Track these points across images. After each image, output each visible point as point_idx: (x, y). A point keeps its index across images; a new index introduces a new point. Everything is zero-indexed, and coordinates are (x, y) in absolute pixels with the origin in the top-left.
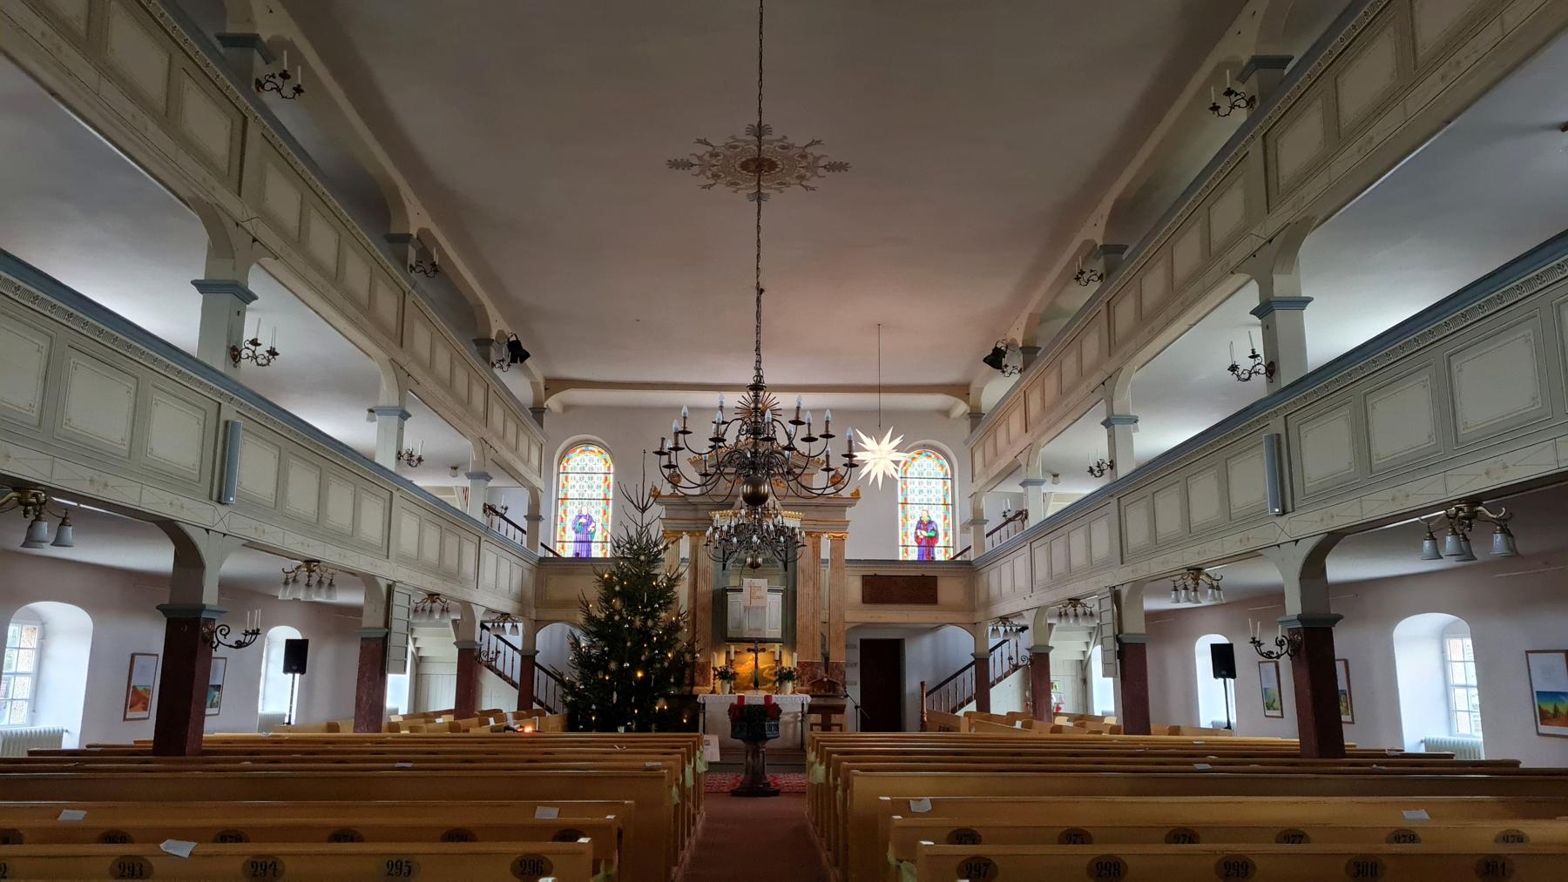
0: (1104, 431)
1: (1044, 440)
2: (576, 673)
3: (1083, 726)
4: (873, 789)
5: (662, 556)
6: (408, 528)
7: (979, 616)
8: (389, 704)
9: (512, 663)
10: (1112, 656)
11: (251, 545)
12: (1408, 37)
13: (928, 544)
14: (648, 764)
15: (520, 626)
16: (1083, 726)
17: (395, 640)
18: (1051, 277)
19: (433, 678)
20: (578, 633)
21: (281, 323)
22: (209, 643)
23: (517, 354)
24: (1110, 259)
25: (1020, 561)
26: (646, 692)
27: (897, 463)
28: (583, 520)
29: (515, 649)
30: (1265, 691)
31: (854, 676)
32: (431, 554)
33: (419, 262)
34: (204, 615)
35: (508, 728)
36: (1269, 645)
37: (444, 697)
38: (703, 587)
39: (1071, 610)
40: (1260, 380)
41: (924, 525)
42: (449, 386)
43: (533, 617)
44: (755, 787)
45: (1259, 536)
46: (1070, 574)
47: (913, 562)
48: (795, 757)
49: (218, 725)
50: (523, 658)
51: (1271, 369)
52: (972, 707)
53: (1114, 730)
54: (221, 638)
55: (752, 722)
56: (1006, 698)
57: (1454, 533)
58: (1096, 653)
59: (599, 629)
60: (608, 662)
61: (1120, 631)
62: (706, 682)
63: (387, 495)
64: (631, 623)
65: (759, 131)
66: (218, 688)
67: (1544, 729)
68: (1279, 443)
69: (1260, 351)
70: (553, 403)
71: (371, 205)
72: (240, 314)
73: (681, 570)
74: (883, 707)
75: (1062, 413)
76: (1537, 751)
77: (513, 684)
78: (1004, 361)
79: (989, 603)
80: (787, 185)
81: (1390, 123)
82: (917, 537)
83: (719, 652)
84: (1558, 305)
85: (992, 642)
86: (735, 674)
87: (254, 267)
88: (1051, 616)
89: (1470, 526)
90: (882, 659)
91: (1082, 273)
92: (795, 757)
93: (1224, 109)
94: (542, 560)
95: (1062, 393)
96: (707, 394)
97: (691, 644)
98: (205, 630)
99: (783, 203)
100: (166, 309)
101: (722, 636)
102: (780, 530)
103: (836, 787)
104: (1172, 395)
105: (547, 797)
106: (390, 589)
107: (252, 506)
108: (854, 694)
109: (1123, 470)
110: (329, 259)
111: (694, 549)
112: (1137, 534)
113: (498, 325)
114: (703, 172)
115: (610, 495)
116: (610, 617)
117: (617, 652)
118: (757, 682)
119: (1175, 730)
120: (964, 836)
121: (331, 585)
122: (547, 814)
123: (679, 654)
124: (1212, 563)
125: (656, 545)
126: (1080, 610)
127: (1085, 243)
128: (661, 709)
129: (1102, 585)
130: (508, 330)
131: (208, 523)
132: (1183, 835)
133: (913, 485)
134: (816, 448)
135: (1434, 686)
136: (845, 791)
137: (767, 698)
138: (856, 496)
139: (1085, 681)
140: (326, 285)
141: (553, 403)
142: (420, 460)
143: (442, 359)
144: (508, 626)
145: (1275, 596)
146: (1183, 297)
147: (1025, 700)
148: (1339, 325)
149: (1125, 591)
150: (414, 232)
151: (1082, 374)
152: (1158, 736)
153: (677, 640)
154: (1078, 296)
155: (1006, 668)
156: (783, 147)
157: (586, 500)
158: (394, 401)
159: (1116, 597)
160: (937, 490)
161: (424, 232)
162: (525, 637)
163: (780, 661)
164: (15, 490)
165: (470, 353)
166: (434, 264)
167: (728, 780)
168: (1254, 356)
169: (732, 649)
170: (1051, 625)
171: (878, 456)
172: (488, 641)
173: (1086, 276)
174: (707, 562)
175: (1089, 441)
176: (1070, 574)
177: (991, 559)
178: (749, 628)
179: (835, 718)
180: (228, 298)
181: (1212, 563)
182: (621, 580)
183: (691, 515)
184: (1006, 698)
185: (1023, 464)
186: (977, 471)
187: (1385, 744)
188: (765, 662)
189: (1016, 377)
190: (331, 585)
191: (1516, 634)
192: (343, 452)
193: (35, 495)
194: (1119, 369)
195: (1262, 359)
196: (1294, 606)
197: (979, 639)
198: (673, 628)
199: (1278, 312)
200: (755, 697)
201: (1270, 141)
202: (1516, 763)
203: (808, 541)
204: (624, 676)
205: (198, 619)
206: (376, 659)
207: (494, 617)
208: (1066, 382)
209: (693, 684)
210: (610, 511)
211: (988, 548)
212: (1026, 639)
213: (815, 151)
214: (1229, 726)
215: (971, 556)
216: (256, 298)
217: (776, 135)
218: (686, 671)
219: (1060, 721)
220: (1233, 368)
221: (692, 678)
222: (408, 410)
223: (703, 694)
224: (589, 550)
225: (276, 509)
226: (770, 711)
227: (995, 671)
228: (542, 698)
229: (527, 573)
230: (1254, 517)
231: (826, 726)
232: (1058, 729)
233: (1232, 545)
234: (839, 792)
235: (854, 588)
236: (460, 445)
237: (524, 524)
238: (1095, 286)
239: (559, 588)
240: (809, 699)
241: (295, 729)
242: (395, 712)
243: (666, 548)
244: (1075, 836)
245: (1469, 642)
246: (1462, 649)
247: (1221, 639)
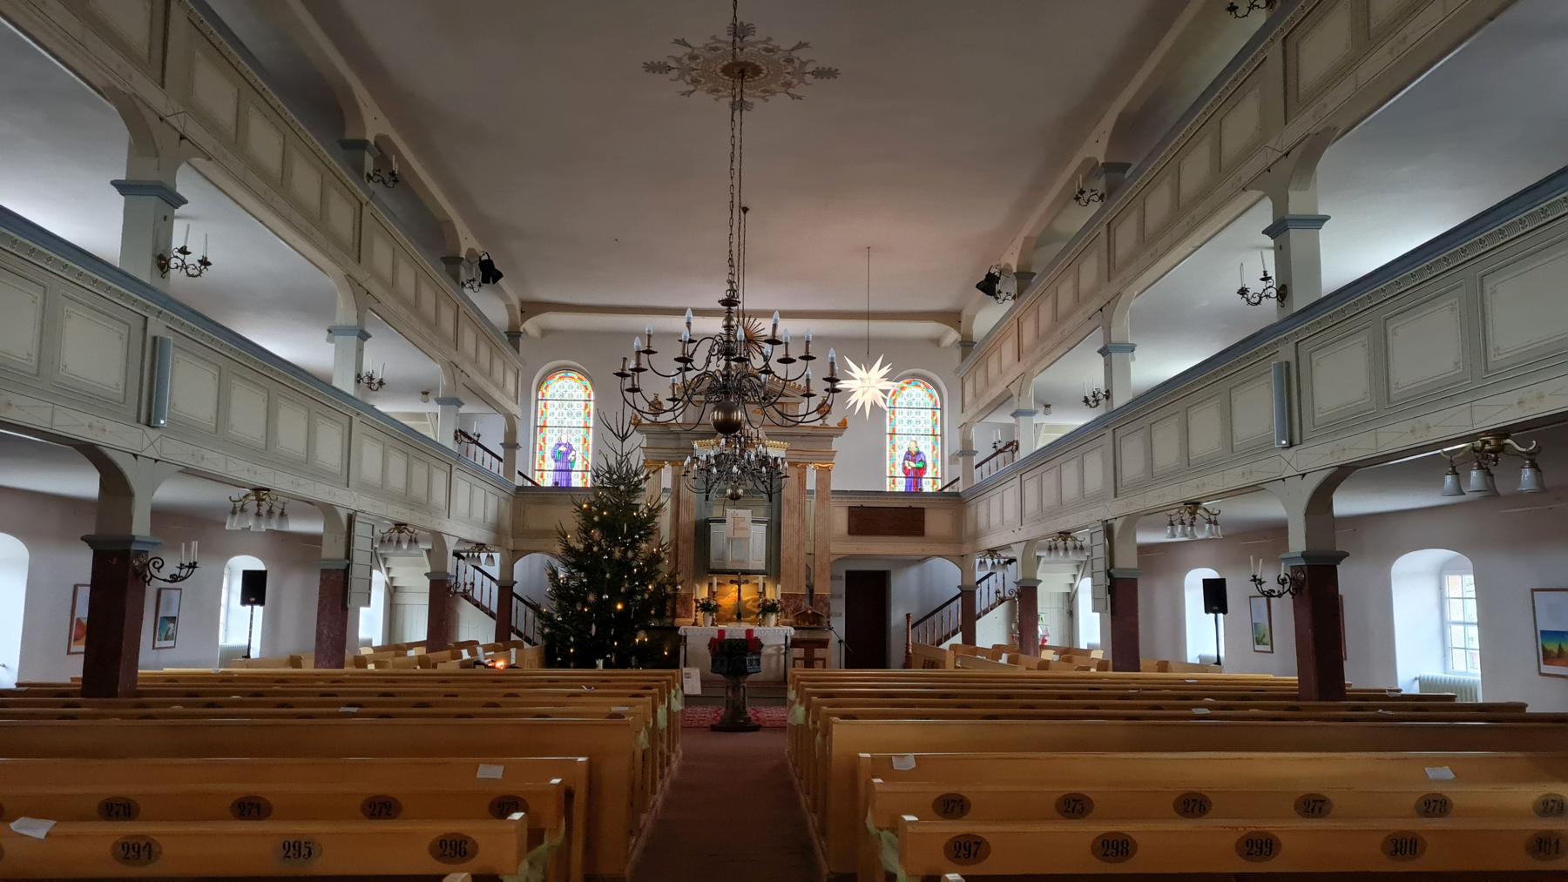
0: (1101, 360)
1: (1037, 369)
2: (555, 605)
3: (1069, 660)
4: (853, 738)
5: (643, 486)
6: (370, 458)
7: (966, 549)
8: (363, 634)
9: (488, 593)
10: (1103, 591)
11: (189, 472)
12: (1177, 188)
13: (915, 475)
14: (615, 709)
15: (497, 556)
16: (1069, 660)
17: (357, 572)
18: (1042, 208)
20: (556, 563)
21: (219, 237)
22: (142, 578)
23: (490, 274)
24: (1112, 176)
25: (1010, 494)
26: (626, 624)
27: (885, 392)
28: (563, 449)
29: (492, 579)
30: (1255, 626)
32: (397, 481)
34: (134, 547)
35: (478, 663)
36: (1271, 583)
37: (417, 628)
38: (687, 518)
39: (1061, 543)
40: (1271, 304)
41: (912, 455)
42: (415, 306)
43: (511, 546)
44: (736, 722)
45: (1263, 470)
46: (1061, 507)
47: (900, 493)
48: (776, 690)
49: (156, 660)
50: (501, 589)
51: (1283, 293)
52: (957, 639)
53: (1102, 666)
55: (733, 657)
56: (992, 630)
57: (1480, 467)
58: (1085, 587)
59: (576, 560)
60: (586, 594)
61: (1112, 566)
62: (688, 613)
63: (345, 420)
64: (610, 554)
65: (739, 31)
66: (173, 619)
67: (1546, 669)
68: (1288, 369)
69: (1272, 273)
70: (530, 326)
71: (320, 107)
72: (167, 220)
73: (663, 500)
74: (869, 644)
75: (1056, 341)
76: (1544, 695)
77: (491, 615)
78: (998, 287)
79: (976, 536)
80: (772, 93)
81: (1344, 90)
82: (905, 468)
83: (701, 583)
85: (979, 575)
86: (717, 607)
87: (184, 168)
88: (1040, 549)
89: (1496, 460)
90: (868, 590)
91: (1082, 192)
92: (776, 690)
93: (1242, 11)
94: (518, 488)
95: (1057, 320)
96: (685, 312)
97: (672, 576)
98: (136, 563)
99: (770, 113)
100: (87, 218)
101: (705, 567)
102: (764, 460)
103: (816, 731)
104: (1170, 324)
105: (492, 751)
106: (351, 519)
107: (186, 430)
108: (838, 626)
109: (1119, 400)
110: (272, 161)
111: (676, 480)
112: (1132, 466)
113: (468, 242)
114: (681, 76)
115: (591, 424)
116: (589, 547)
117: (595, 584)
118: (739, 614)
119: (1163, 666)
120: (952, 806)
121: (282, 514)
122: (490, 771)
123: (660, 586)
124: (1208, 498)
125: (636, 475)
126: (1070, 543)
127: (1086, 161)
128: (642, 642)
129: (1093, 519)
130: (479, 249)
131: (137, 449)
132: (1193, 804)
133: (901, 415)
134: (793, 371)
135: (1432, 625)
136: (824, 736)
137: (749, 632)
138: (843, 425)
139: (1071, 614)
140: (270, 193)
141: (530, 326)
142: (381, 383)
143: (406, 279)
144: (483, 556)
145: (1278, 531)
146: (1190, 217)
147: (1011, 633)
148: (1354, 249)
149: (1117, 525)
151: (1078, 300)
152: (1147, 673)
153: (659, 572)
154: (1077, 218)
155: (993, 600)
156: (767, 50)
157: (566, 425)
158: (353, 321)
159: (1109, 531)
160: (926, 420)
161: (382, 141)
162: (502, 567)
163: (764, 592)
166: (393, 174)
167: (710, 713)
168: (1266, 278)
169: (715, 581)
170: (1039, 558)
171: (865, 385)
172: (467, 574)
173: (1086, 196)
174: (691, 496)
175: (1085, 371)
176: (1061, 507)
177: (979, 491)
178: (732, 560)
179: (819, 653)
180: (151, 203)
181: (1208, 498)
182: (600, 510)
183: (672, 444)
184: (992, 630)
185: (1015, 394)
186: (967, 400)
187: (1378, 683)
188: (748, 594)
189: (1010, 303)
190: (282, 514)
191: (1521, 573)
192: (293, 373)
194: (1119, 294)
195: (1273, 282)
196: (1297, 543)
197: (967, 571)
198: (654, 559)
199: (1293, 232)
200: (736, 630)
202: (1522, 707)
203: (793, 473)
204: (603, 608)
206: (338, 596)
207: (468, 547)
208: (1151, 224)
209: (674, 616)
210: (590, 439)
211: (977, 480)
212: (1013, 574)
213: (802, 55)
214: (1218, 662)
215: (959, 487)
216: (185, 202)
217: (760, 35)
218: (667, 604)
219: (1047, 655)
220: (1243, 291)
221: (674, 610)
222: (367, 330)
223: (685, 626)
224: (569, 480)
225: (219, 432)
226: (752, 645)
227: (981, 603)
228: (521, 628)
230: (1259, 450)
231: (809, 662)
232: (1045, 665)
233: (1234, 479)
234: (819, 738)
235: (840, 520)
236: (426, 368)
237: (500, 452)
238: (1095, 207)
239: (538, 518)
240: (791, 631)
241: (257, 663)
242: (368, 643)
243: (647, 478)
244: (1074, 806)
245: (1470, 578)
246: (1462, 586)
247: (1212, 574)
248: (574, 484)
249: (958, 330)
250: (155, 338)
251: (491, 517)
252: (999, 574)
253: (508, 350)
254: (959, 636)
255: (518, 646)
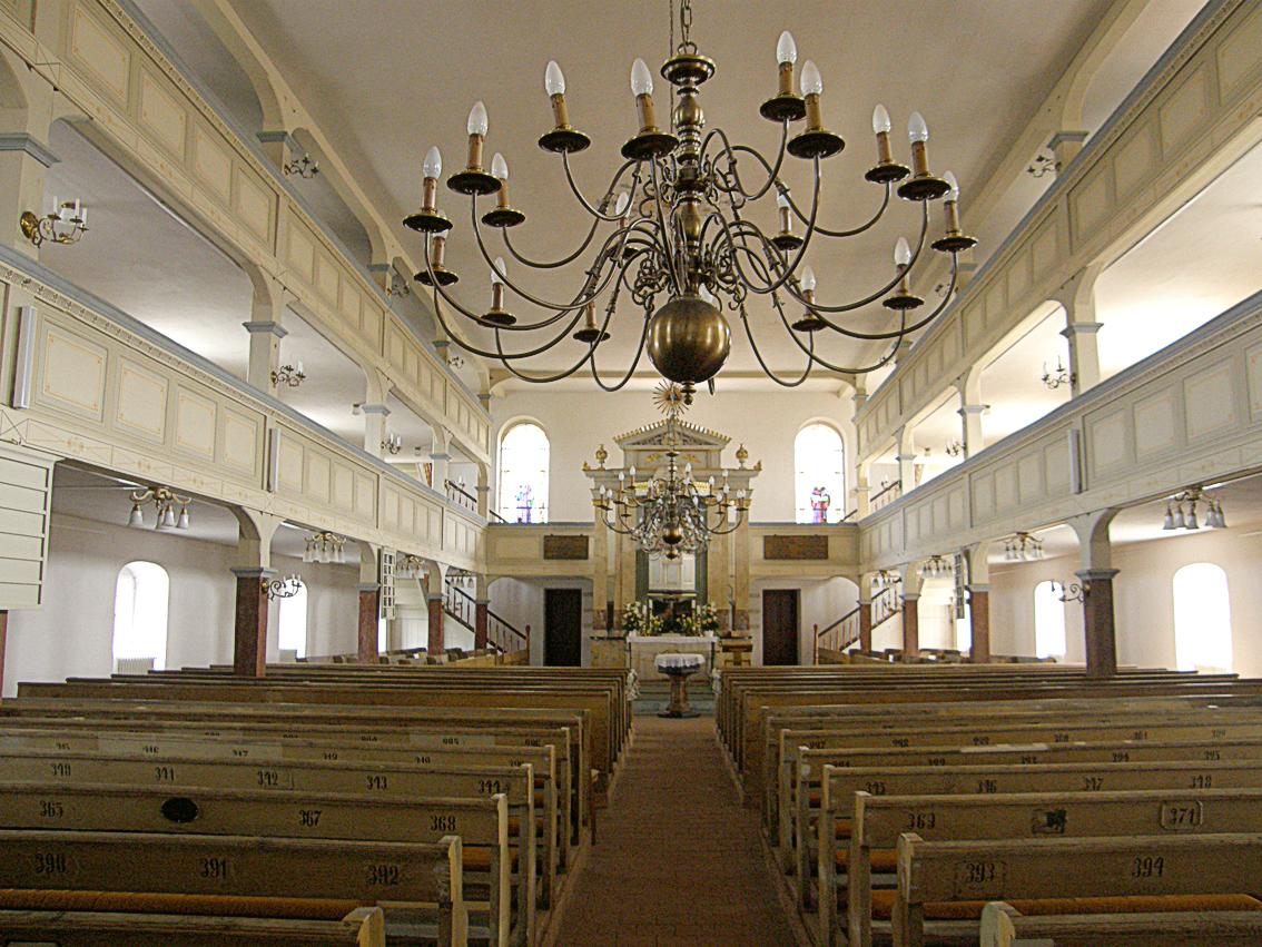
12: (1158, 137)
19: (404, 623)
29: (470, 599)
31: (757, 619)
32: (407, 523)
33: (394, 287)
34: (263, 575)
39: (933, 564)
41: (818, 491)
51: (1074, 380)
54: (275, 591)
56: (886, 637)
63: (375, 477)
68: (1078, 436)
77: (470, 628)
79: (872, 558)
84: (1246, 349)
85: (875, 592)
90: (783, 607)
126: (941, 564)
138: (758, 468)
141: (497, 389)
144: (466, 579)
150: (390, 263)
164: (150, 489)
165: (431, 353)
166: (406, 288)
179: (744, 656)
186: (862, 445)
193: (164, 493)
194: (970, 369)
195: (1068, 371)
201: (966, 312)
202: (1236, 676)
205: (258, 579)
229: (479, 535)
239: (504, 547)
248: (533, 521)
249: (854, 385)
250: (271, 431)
251: (472, 548)
252: (892, 591)
253: (480, 409)
254: (858, 642)
255: (493, 652)
